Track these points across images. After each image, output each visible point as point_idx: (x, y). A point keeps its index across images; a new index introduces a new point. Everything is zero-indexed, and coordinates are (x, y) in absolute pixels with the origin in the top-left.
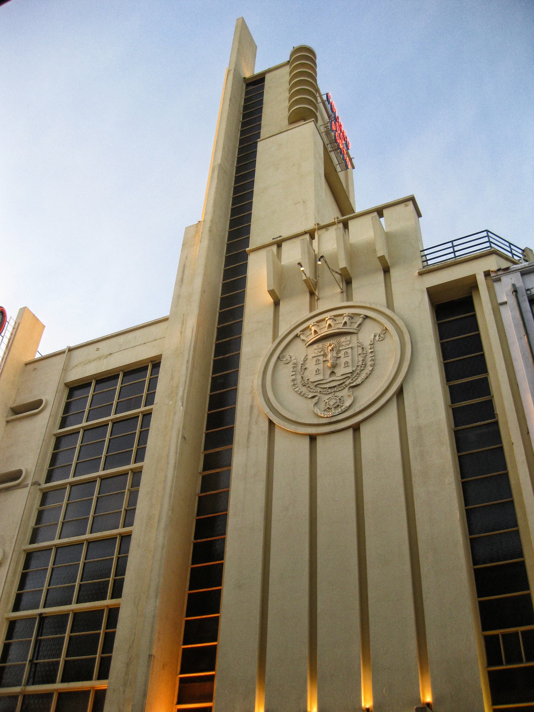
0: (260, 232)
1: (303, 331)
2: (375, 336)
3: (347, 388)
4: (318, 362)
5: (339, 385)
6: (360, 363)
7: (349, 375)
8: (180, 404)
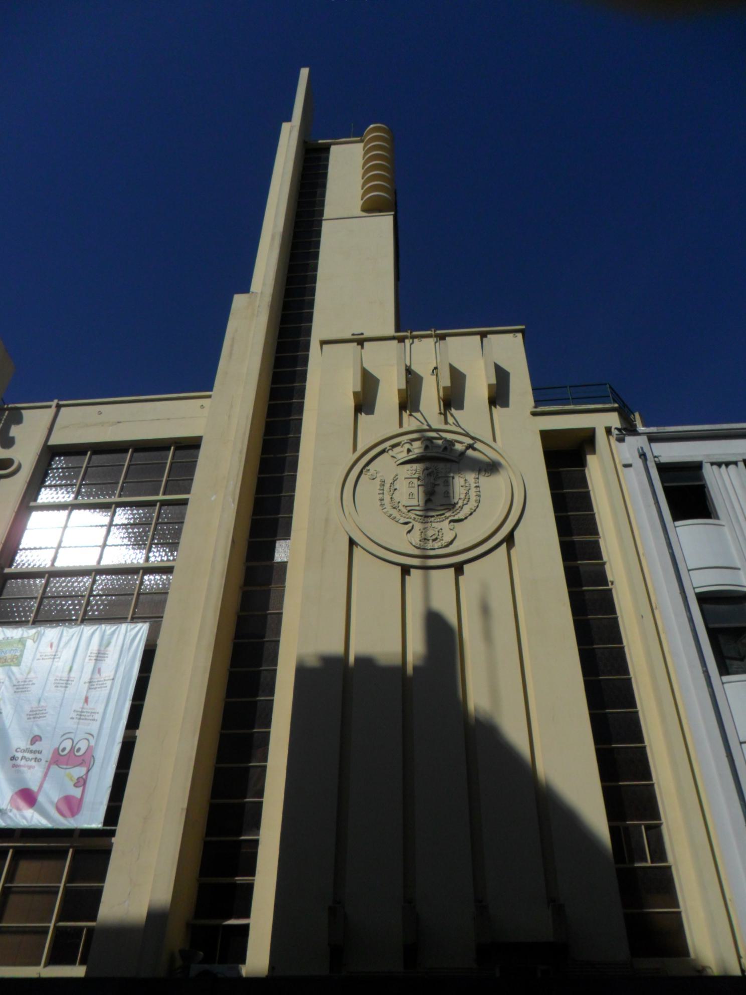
0: (322, 324)
1: (394, 446)
3: (448, 521)
6: (463, 496)
8: (231, 500)
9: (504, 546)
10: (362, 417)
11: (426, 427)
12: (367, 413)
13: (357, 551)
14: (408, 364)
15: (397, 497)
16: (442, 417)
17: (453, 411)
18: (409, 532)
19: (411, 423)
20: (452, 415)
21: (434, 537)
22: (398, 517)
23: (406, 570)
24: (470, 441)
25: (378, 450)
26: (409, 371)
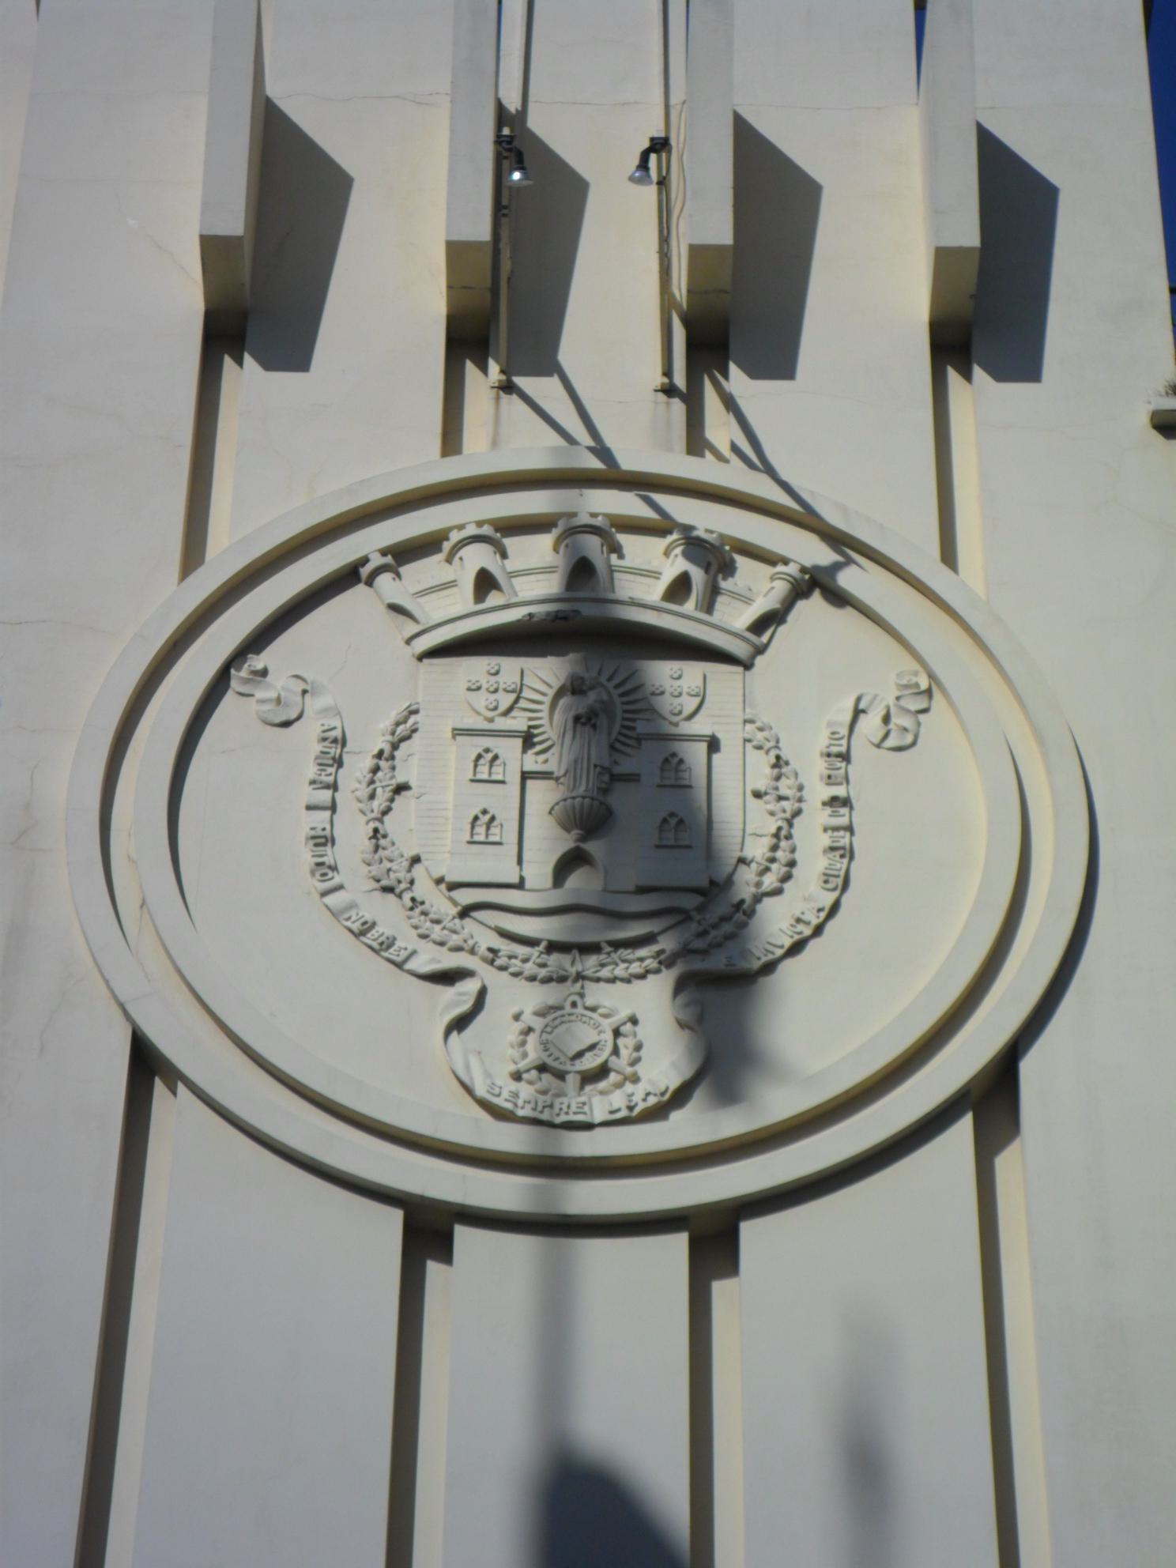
1: (405, 553)
2: (858, 712)
7: (689, 902)
9: (964, 1128)
10: (246, 381)
11: (595, 463)
12: (270, 364)
13: (169, 1110)
14: (513, 104)
15: (406, 827)
16: (678, 407)
17: (737, 380)
18: (460, 1024)
19: (507, 432)
20: (730, 403)
21: (590, 1062)
22: (407, 940)
23: (429, 1231)
24: (820, 554)
25: (325, 566)
26: (514, 143)
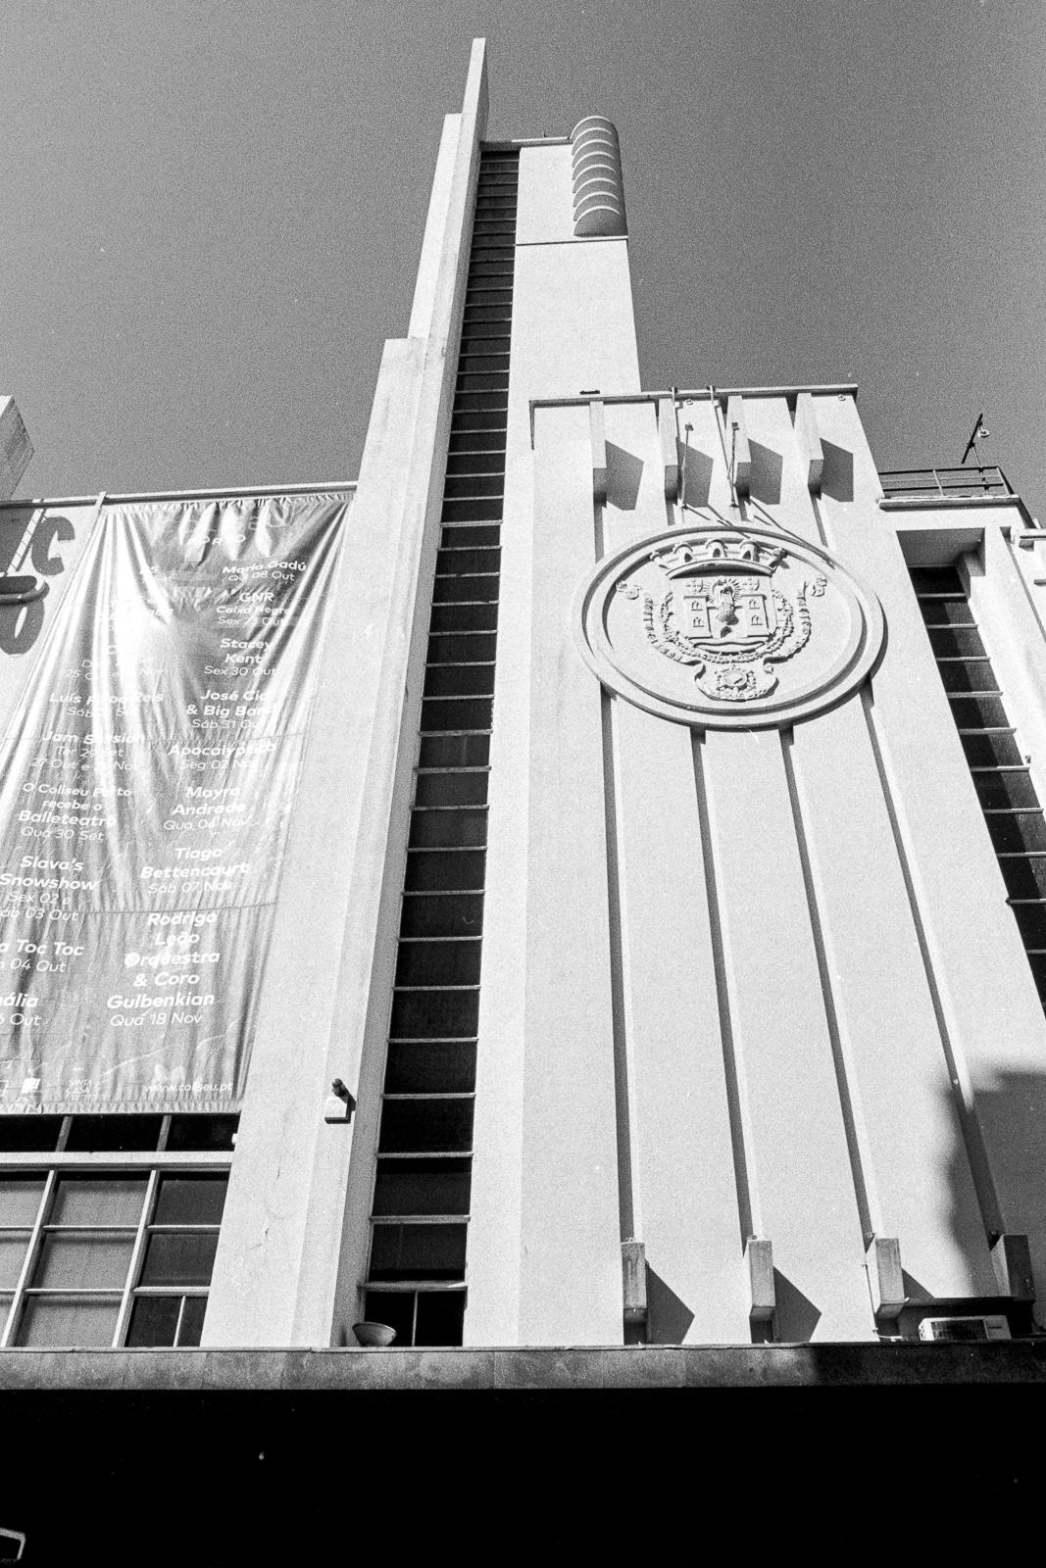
4: (695, 608)
5: (743, 652)
7: (765, 639)
